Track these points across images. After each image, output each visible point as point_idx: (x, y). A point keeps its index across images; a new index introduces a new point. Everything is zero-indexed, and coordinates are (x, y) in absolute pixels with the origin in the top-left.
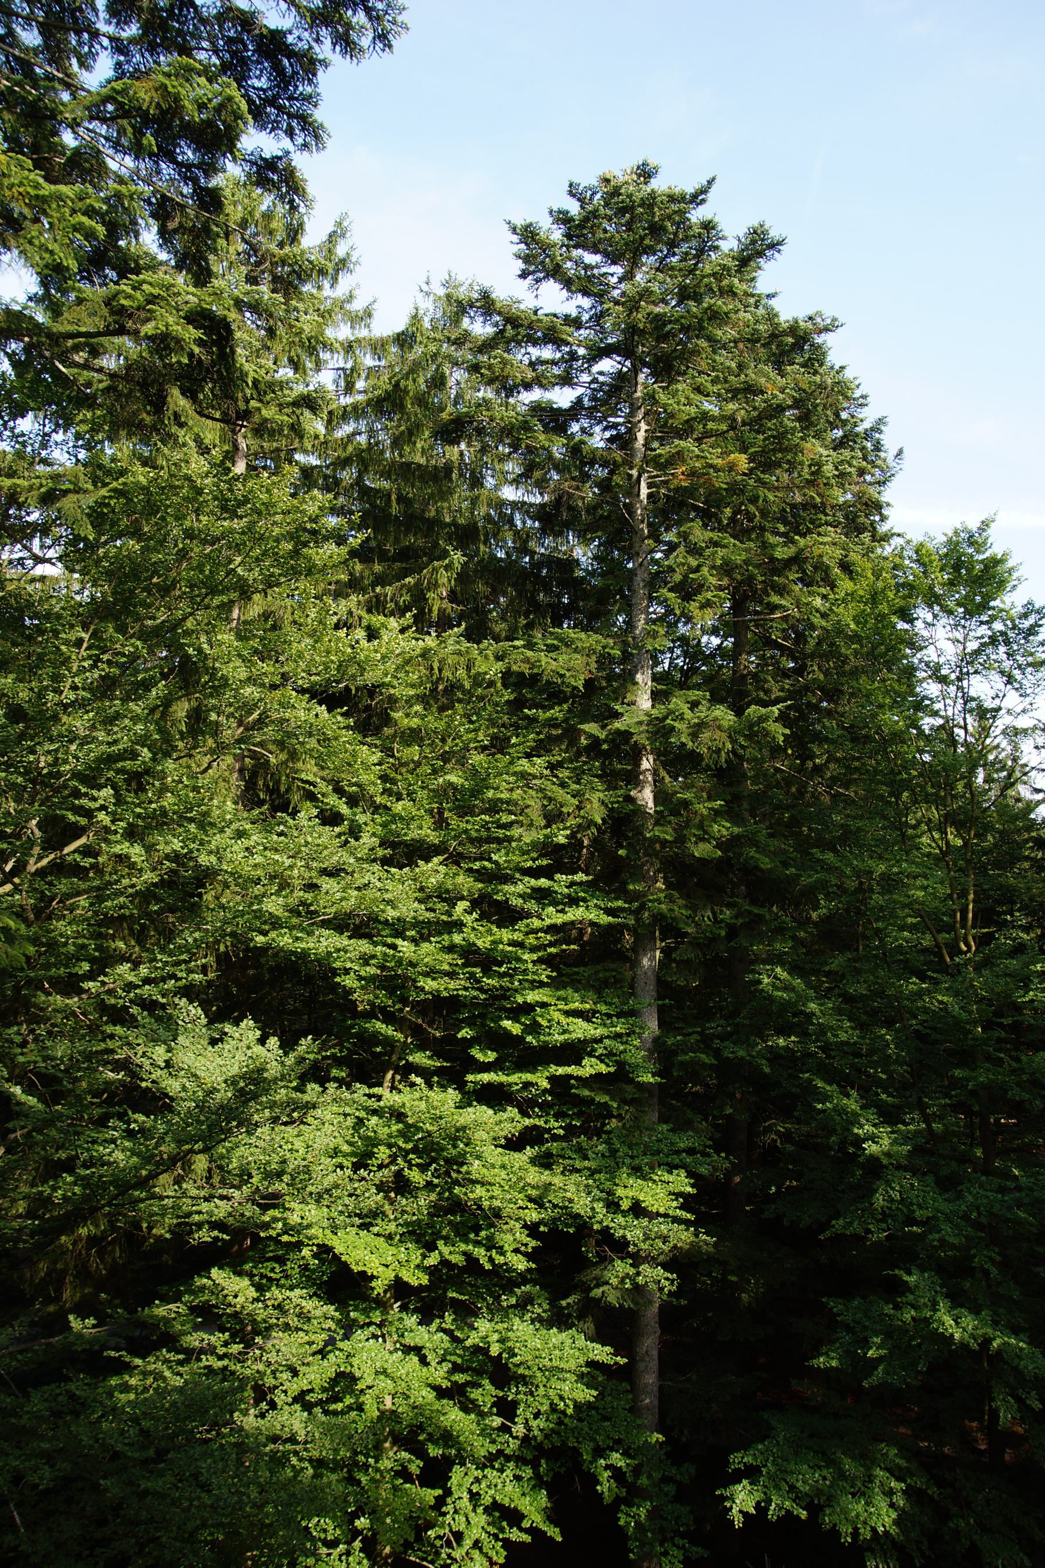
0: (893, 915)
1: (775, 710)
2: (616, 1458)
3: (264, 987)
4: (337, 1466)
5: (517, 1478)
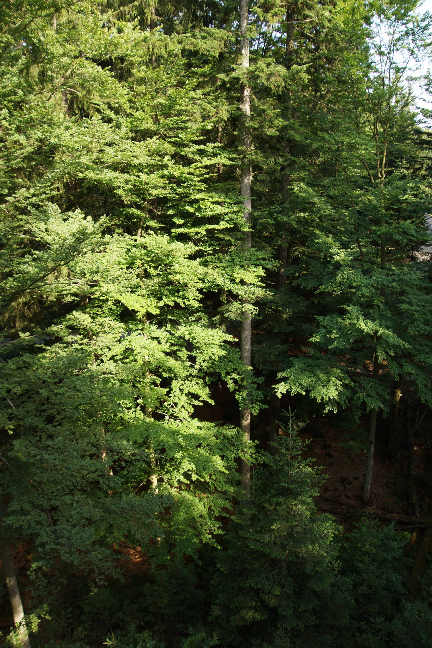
0: (351, 161)
1: (305, 67)
2: (235, 376)
3: (84, 196)
4: (128, 382)
5: (197, 383)
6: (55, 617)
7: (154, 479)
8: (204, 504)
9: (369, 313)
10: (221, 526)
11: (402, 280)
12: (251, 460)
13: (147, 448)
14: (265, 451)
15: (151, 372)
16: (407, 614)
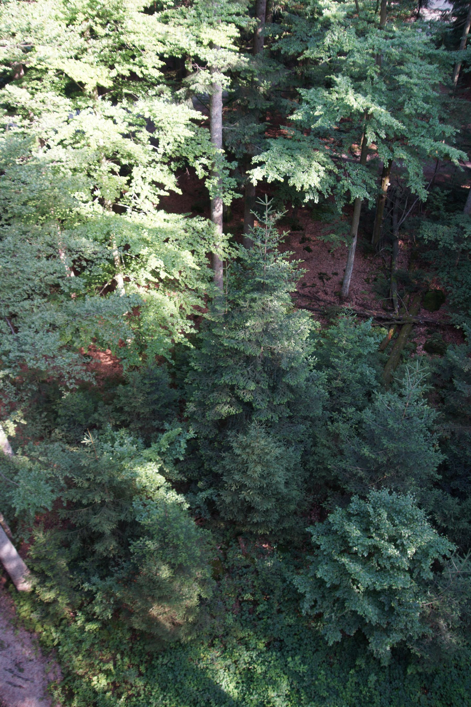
2: (204, 160)
5: (162, 170)
6: (30, 421)
7: (119, 278)
8: (175, 303)
9: (360, 87)
10: (194, 325)
11: (403, 44)
12: (224, 255)
13: (109, 245)
14: (238, 244)
15: (107, 158)
16: (377, 404)
